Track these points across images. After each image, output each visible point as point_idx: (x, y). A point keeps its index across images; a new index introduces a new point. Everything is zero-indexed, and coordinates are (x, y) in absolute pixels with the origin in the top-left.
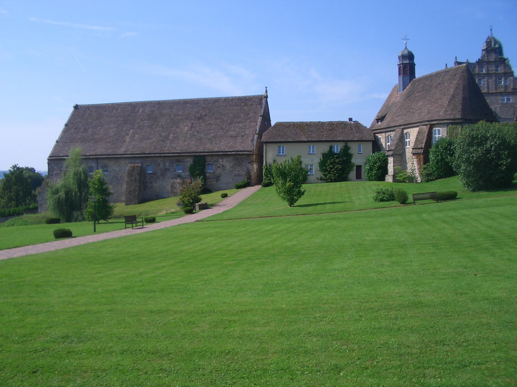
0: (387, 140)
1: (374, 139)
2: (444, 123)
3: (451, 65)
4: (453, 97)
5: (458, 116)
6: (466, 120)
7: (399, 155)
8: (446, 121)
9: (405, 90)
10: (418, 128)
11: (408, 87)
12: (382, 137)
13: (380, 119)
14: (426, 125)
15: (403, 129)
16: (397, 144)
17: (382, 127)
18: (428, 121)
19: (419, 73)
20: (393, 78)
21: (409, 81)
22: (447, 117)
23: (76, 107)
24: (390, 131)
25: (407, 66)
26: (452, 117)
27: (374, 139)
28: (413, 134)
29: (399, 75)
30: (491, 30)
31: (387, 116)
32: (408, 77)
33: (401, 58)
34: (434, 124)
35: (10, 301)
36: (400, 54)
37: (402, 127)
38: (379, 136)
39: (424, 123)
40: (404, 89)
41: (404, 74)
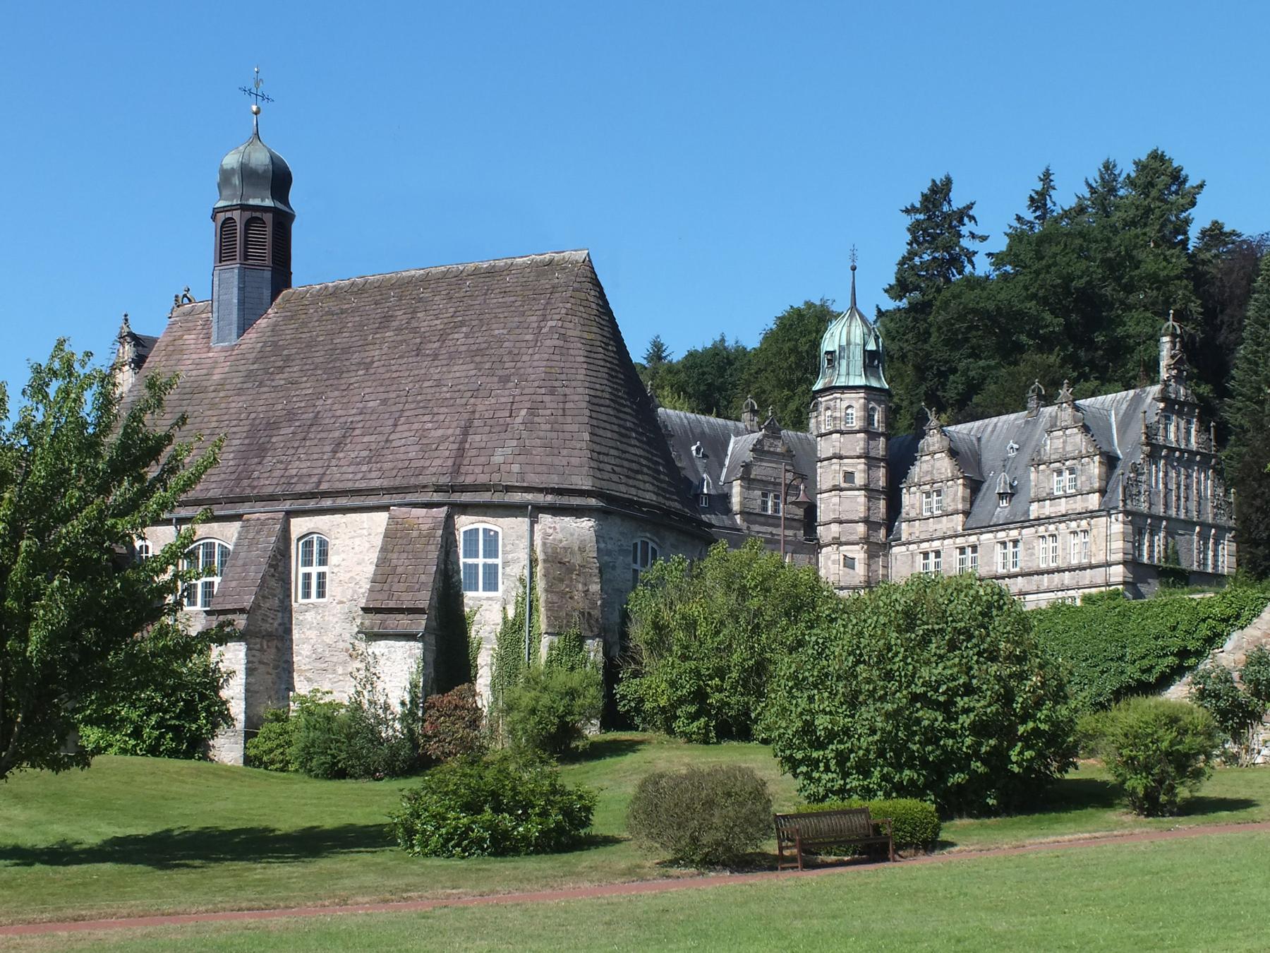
3: (818, 303)
8: (529, 497)
9: (251, 335)
10: (383, 516)
11: (262, 323)
15: (290, 514)
18: (438, 489)
19: (308, 269)
21: (267, 293)
22: (533, 480)
23: (1157, 156)
26: (554, 481)
32: (268, 274)
33: (236, 181)
37: (287, 505)
39: (410, 498)
40: (243, 328)
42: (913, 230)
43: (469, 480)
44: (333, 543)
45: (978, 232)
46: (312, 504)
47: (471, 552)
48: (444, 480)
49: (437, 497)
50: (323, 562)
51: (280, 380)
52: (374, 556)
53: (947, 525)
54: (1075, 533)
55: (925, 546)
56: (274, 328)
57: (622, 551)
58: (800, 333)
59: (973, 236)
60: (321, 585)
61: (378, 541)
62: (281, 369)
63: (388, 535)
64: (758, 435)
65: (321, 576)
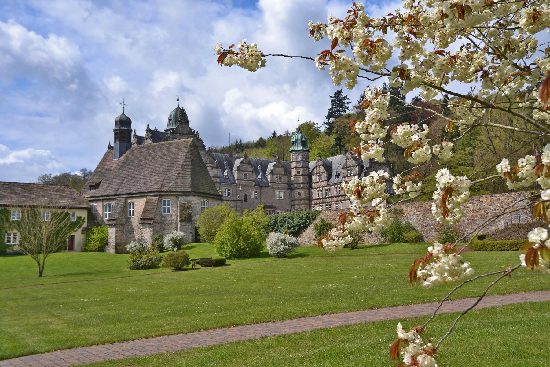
0: (105, 208)
2: (100, 200)
4: (183, 168)
5: (189, 189)
6: (195, 192)
7: (122, 225)
9: (122, 158)
10: (144, 200)
11: (125, 154)
12: (99, 207)
14: (155, 196)
16: (120, 213)
17: (98, 195)
22: (178, 189)
24: (109, 200)
26: (182, 189)
28: (139, 205)
30: (178, 100)
31: (102, 183)
33: (118, 123)
34: (163, 195)
37: (126, 196)
40: (120, 156)
41: (120, 140)
42: (332, 101)
43: (164, 189)
44: (136, 204)
45: (349, 101)
46: (131, 196)
47: (164, 205)
48: (158, 190)
49: (157, 194)
50: (133, 208)
51: (127, 167)
52: (143, 206)
53: (322, 184)
54: (336, 188)
55: (318, 189)
56: (127, 156)
57: (198, 203)
58: (452, 80)
59: (348, 103)
60: (133, 213)
61: (144, 203)
62: (128, 165)
63: (147, 202)
64: (275, 163)
65: (133, 211)
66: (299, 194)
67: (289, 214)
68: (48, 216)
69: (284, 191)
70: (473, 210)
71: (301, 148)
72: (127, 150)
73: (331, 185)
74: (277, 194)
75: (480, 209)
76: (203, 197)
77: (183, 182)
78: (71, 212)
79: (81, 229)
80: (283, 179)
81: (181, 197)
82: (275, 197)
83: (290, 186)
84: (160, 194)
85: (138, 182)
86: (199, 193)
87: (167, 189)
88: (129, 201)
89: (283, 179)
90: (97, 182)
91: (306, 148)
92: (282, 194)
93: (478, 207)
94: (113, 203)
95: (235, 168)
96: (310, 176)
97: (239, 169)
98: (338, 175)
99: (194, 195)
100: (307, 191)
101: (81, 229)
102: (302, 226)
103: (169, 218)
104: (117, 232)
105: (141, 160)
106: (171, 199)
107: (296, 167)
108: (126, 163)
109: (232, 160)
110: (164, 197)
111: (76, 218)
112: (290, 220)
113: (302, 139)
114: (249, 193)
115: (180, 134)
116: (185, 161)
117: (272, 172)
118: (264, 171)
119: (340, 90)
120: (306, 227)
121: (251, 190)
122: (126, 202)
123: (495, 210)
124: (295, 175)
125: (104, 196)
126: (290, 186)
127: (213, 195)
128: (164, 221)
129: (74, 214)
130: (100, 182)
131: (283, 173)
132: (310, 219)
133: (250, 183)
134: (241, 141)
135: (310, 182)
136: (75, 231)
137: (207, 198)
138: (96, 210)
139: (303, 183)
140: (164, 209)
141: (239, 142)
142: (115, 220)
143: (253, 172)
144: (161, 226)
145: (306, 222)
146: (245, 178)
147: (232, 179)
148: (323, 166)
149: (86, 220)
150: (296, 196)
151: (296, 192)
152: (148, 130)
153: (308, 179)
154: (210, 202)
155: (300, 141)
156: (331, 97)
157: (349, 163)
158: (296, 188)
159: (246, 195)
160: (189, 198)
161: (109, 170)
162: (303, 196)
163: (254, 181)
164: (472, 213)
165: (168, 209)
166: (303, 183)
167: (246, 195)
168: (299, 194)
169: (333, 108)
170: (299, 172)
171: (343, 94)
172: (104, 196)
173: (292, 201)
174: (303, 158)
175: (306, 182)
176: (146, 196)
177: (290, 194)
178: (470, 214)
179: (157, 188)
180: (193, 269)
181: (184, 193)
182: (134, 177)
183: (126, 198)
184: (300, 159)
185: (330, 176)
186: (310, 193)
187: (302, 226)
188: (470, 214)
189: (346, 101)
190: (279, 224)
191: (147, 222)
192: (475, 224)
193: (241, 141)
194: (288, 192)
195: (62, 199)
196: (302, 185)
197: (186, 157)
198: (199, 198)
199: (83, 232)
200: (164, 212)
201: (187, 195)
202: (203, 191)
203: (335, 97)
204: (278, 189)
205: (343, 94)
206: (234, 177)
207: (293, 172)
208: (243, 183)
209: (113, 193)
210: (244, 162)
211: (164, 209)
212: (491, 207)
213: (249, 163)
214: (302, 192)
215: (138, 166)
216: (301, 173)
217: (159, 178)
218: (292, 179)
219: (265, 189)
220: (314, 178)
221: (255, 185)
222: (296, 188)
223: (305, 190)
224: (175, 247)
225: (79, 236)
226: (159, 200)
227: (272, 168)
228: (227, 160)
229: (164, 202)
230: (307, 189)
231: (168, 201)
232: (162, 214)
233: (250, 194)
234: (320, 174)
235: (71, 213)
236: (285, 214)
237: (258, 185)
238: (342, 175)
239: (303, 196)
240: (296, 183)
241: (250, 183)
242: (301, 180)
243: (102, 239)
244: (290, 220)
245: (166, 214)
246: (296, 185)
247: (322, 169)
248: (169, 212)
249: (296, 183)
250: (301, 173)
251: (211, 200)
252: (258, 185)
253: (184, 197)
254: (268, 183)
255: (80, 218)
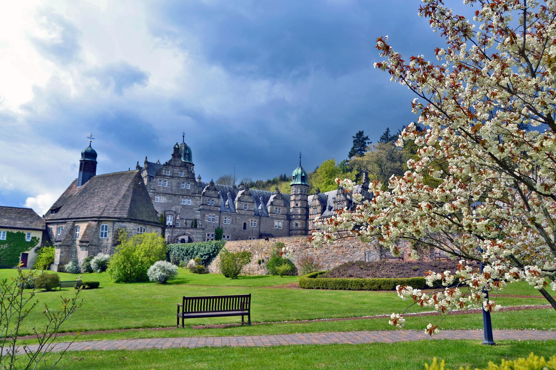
0: (58, 229)
1: (45, 228)
4: (125, 196)
5: (126, 216)
6: (131, 219)
7: (67, 246)
9: (84, 185)
12: (54, 229)
13: (55, 209)
14: (95, 221)
17: (55, 218)
19: (99, 172)
20: (75, 174)
22: (116, 216)
25: (89, 163)
26: (120, 216)
27: (45, 228)
28: (82, 227)
29: (80, 170)
34: (102, 221)
35: (209, 216)
36: (84, 151)
38: (50, 226)
40: (82, 184)
41: (84, 170)
42: (354, 141)
45: (369, 141)
57: (134, 229)
59: (368, 143)
63: (88, 226)
66: (297, 225)
67: (202, 244)
68: (3, 235)
69: (283, 221)
70: (337, 247)
71: (300, 183)
72: (89, 179)
73: (324, 217)
74: (276, 223)
75: (342, 246)
76: (140, 224)
77: (121, 210)
78: (26, 232)
79: (35, 248)
80: (283, 210)
81: (117, 223)
82: (273, 226)
83: (289, 217)
84: (99, 220)
85: (87, 208)
86: (136, 220)
87: (106, 215)
88: (76, 225)
89: (283, 210)
90: (58, 207)
91: (305, 182)
92: (281, 224)
93: (341, 245)
94: (64, 226)
95: (236, 199)
96: (307, 208)
97: (239, 200)
98: (330, 209)
99: (130, 222)
100: (304, 222)
101: (35, 248)
102: (211, 254)
103: (105, 242)
104: (61, 253)
105: (96, 189)
106: (109, 225)
107: (295, 200)
108: (84, 191)
109: (236, 192)
110: (103, 222)
111: (31, 238)
112: (203, 248)
113: (302, 174)
114: (249, 222)
115: (173, 166)
116: (128, 190)
117: (272, 204)
118: (265, 202)
119: (361, 131)
120: (214, 256)
121: (250, 220)
122: (73, 225)
123: (353, 247)
124: (294, 207)
125: (59, 219)
126: (289, 217)
127: (151, 222)
128: (101, 244)
129: (29, 234)
130: (61, 207)
131: (283, 205)
132: (217, 249)
133: (249, 213)
134: (285, 175)
135: (307, 215)
136: (29, 250)
137: (145, 224)
138: (52, 232)
139: (300, 215)
140: (102, 233)
141: (283, 176)
142: (60, 241)
143: (253, 203)
144: (98, 249)
145: (215, 251)
146: (245, 208)
147: (232, 208)
148: (318, 199)
149: (40, 241)
150: (294, 226)
151: (294, 222)
152: (146, 162)
153: (305, 211)
154: (148, 228)
155: (300, 176)
156: (354, 137)
157: (339, 197)
158: (294, 219)
159: (245, 224)
160: (124, 224)
161: (71, 196)
162: (299, 226)
163: (254, 211)
164: (336, 250)
165: (106, 233)
166: (300, 215)
167: (245, 224)
168: (297, 225)
169: (354, 147)
170: (297, 205)
171: (365, 135)
172: (59, 219)
173: (290, 230)
174: (301, 191)
175: (304, 214)
176: (88, 221)
177: (289, 225)
178: (335, 251)
179: (98, 214)
180: (60, 290)
181: (120, 220)
182: (85, 203)
183: (74, 222)
184: (299, 193)
185: (324, 209)
186: (307, 224)
187: (211, 254)
188: (335, 251)
189: (367, 141)
190: (195, 252)
191: (84, 244)
192: (337, 261)
193: (285, 175)
194: (287, 222)
195: (20, 221)
196: (299, 217)
197: (129, 187)
198: (136, 225)
199: (36, 251)
200: (102, 236)
201: (123, 222)
202: (141, 218)
203: (357, 137)
204: (277, 219)
205: (365, 135)
206: (235, 207)
207: (292, 204)
208: (242, 212)
209: (66, 217)
210: (245, 193)
211: (102, 233)
212: (350, 244)
213: (250, 195)
214: (299, 222)
215: (92, 193)
216: (299, 205)
217: (102, 205)
218: (291, 210)
219: (264, 219)
220: (311, 210)
221: (255, 215)
222: (294, 219)
223: (302, 221)
224: (98, 268)
225: (31, 253)
226: (98, 225)
227: (272, 200)
228: (230, 191)
229: (103, 226)
230: (304, 220)
231: (106, 226)
232: (100, 238)
233: (249, 223)
234: (315, 207)
235: (26, 234)
236: (200, 243)
237: (258, 215)
238: (333, 209)
239: (299, 226)
240: (294, 215)
241: (249, 213)
242: (299, 211)
243: (51, 258)
244: (203, 248)
245: (104, 238)
246: (294, 217)
247: (317, 202)
248: (106, 236)
249: (294, 215)
250: (299, 205)
251: (148, 227)
252: (258, 215)
253: (121, 224)
254: (268, 213)
255: (34, 238)
